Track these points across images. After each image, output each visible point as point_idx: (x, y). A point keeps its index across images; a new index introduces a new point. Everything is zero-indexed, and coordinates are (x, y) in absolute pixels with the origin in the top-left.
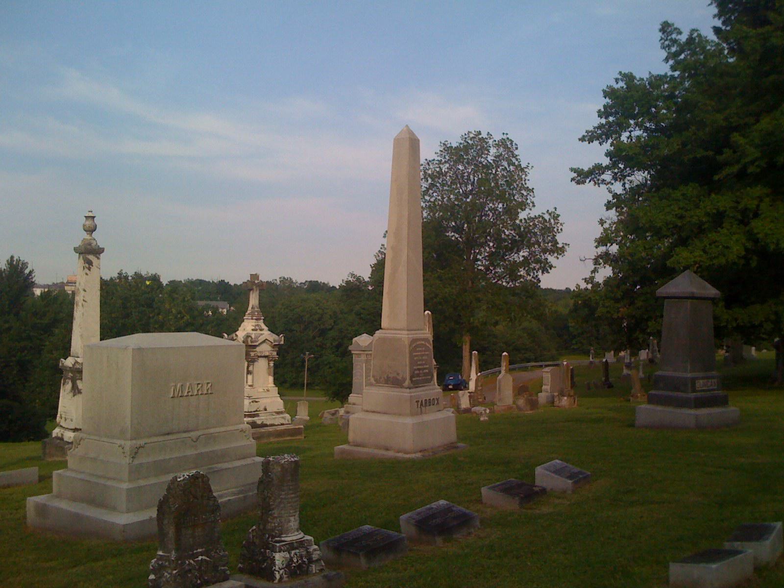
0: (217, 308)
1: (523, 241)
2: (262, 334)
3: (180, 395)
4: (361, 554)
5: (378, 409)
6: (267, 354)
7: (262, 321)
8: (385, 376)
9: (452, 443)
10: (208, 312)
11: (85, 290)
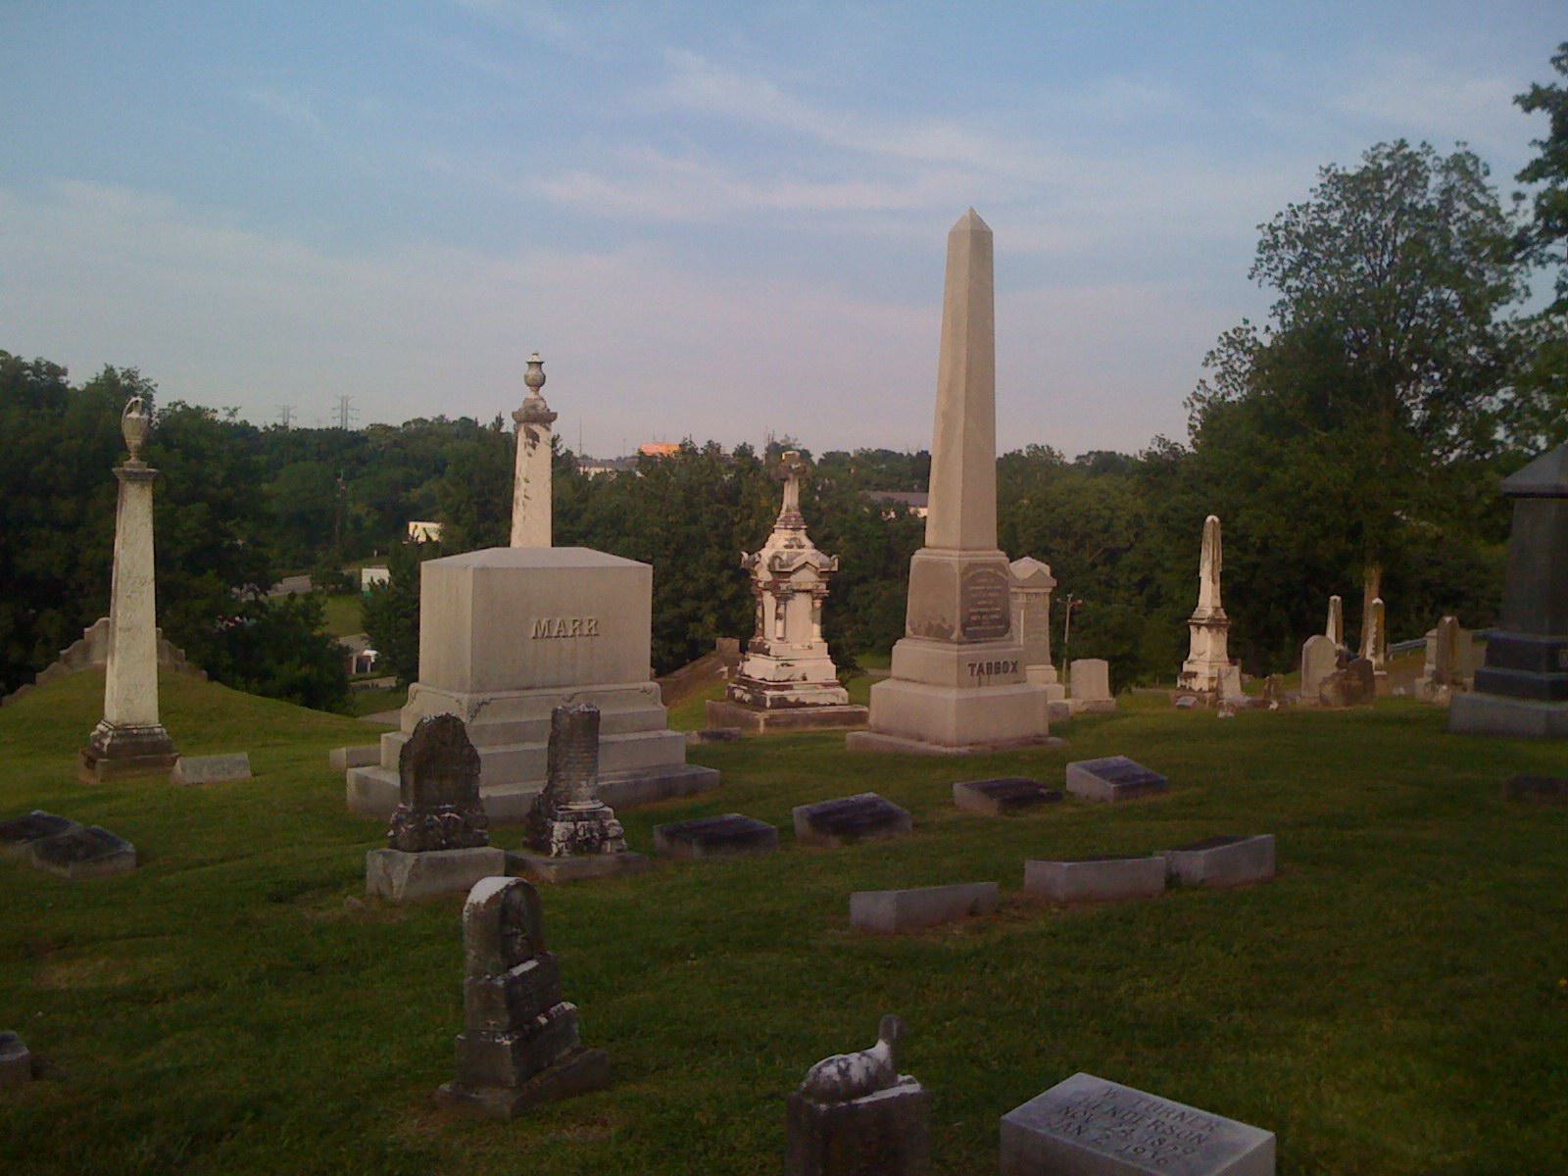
0: (907, 506)
1: (1503, 369)
2: (799, 554)
3: (546, 635)
4: (694, 840)
5: (914, 677)
6: (810, 587)
7: (803, 532)
8: (927, 623)
9: (1039, 736)
10: (888, 513)
11: (527, 481)
